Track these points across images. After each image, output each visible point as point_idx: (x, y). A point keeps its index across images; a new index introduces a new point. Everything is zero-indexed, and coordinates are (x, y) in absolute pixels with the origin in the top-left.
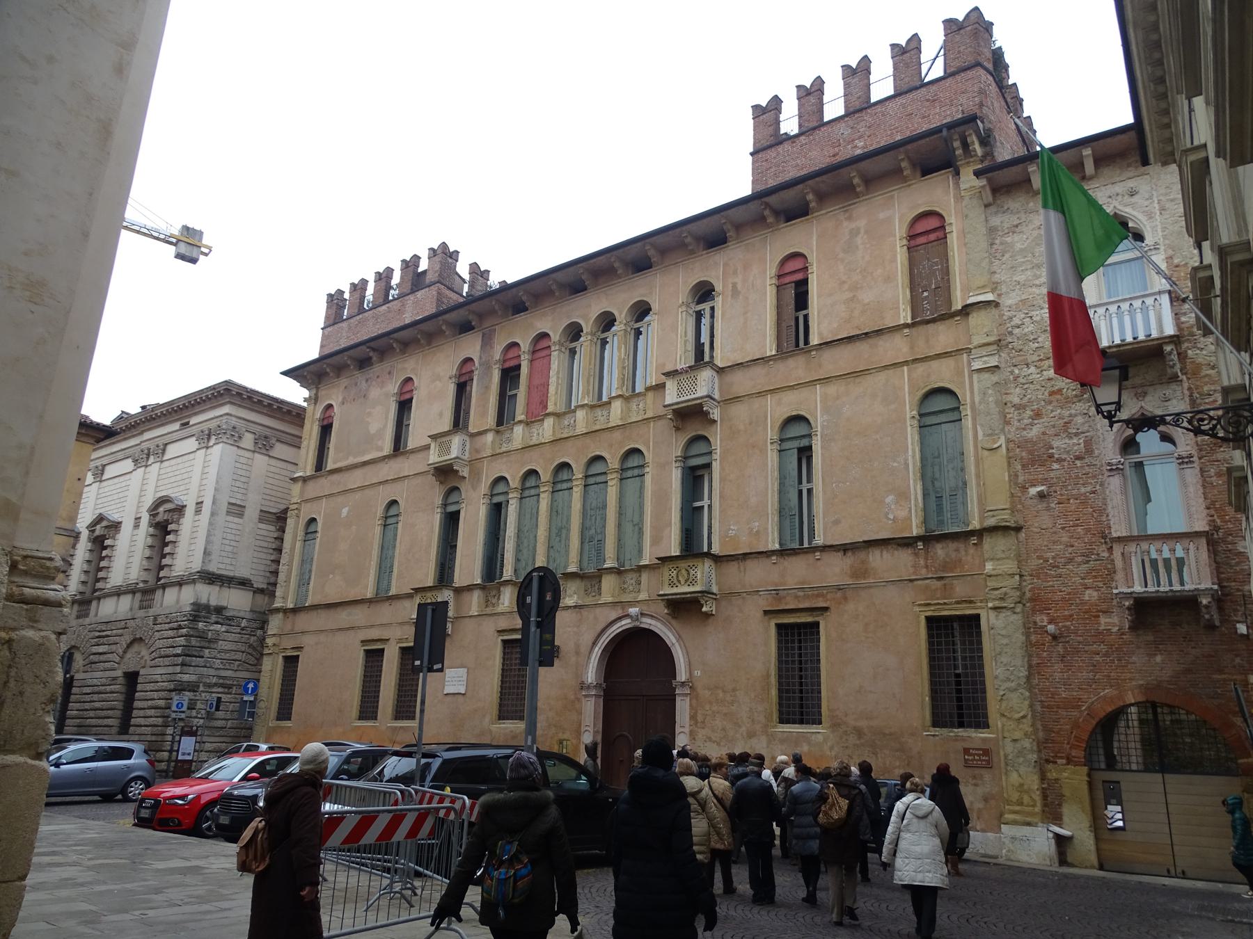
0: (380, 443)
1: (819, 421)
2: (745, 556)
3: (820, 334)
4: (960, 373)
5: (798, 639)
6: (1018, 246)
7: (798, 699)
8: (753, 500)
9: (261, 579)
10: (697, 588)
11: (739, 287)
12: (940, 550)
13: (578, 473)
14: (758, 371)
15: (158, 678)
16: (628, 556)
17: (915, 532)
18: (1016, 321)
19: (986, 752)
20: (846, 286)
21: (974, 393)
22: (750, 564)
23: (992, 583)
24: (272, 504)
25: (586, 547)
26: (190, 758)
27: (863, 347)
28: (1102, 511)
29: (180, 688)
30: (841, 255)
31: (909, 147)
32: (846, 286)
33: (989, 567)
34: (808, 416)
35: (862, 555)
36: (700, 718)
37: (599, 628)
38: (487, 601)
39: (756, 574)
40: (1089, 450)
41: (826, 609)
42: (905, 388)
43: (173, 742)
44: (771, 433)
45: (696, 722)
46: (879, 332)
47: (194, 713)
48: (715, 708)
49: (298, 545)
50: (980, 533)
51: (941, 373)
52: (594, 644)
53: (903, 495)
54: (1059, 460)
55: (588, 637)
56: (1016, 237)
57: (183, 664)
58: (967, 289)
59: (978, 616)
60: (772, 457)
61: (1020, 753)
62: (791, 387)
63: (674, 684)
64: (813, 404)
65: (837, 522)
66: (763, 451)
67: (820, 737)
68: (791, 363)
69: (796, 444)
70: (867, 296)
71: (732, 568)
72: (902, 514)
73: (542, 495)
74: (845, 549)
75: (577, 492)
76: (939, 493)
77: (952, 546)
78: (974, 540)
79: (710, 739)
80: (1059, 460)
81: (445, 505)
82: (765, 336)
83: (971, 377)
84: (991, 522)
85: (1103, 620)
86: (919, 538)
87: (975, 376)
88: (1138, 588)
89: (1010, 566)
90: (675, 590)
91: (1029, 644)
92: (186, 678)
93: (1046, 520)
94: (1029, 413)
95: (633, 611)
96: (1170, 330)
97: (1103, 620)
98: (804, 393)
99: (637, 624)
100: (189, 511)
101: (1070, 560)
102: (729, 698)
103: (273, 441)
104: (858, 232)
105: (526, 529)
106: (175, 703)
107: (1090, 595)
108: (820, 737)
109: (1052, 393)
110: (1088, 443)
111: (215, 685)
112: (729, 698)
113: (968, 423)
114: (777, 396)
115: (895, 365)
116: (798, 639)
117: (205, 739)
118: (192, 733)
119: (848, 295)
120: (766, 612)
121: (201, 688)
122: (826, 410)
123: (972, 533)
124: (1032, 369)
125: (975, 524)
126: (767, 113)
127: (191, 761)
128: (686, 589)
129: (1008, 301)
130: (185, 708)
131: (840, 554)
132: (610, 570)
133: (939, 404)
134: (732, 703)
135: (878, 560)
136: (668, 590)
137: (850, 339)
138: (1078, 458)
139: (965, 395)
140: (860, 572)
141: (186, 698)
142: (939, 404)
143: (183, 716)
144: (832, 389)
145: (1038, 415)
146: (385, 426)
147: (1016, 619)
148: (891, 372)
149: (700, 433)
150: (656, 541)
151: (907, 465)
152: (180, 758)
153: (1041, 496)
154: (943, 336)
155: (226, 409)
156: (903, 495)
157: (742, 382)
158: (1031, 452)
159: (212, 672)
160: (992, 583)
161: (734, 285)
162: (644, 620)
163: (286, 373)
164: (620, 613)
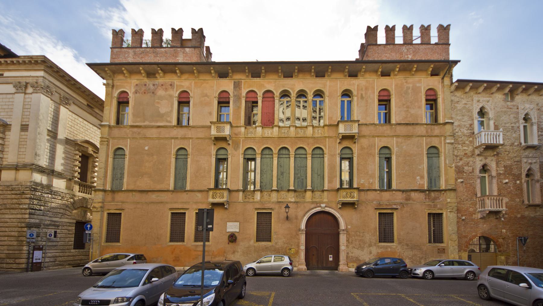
0: (169, 119)
1: (395, 150)
2: (368, 190)
3: (396, 120)
4: (441, 143)
5: (386, 218)
6: (458, 108)
7: (386, 234)
8: (370, 172)
9: (69, 174)
10: (355, 199)
11: (364, 95)
12: (433, 194)
13: (292, 152)
14: (372, 128)
15: (8, 220)
16: (316, 186)
17: (426, 188)
18: (457, 131)
19: (444, 249)
20: (405, 106)
21: (445, 150)
22: (369, 192)
23: (449, 205)
24: (72, 136)
25: (296, 181)
26: (40, 261)
27: (410, 127)
28: (475, 188)
29: (30, 226)
30: (403, 95)
31: (437, 64)
32: (405, 106)
33: (449, 200)
34: (391, 147)
35: (409, 193)
36: (350, 241)
37: (306, 210)
38: (246, 197)
39: (371, 195)
40: (473, 171)
41: (397, 209)
42: (425, 144)
43: (29, 253)
44: (377, 151)
45: (349, 242)
46: (417, 124)
47: (39, 239)
48: (356, 238)
49: (110, 160)
50: (445, 190)
51: (435, 142)
52: (304, 216)
53: (422, 177)
54: (466, 173)
55: (300, 213)
56: (458, 105)
57: (30, 214)
58: (445, 117)
59: (442, 214)
60: (377, 159)
61: (454, 249)
62: (385, 136)
63: (339, 230)
64: (393, 143)
65: (400, 183)
66: (374, 156)
67: (395, 247)
68: (385, 128)
69: (384, 156)
70: (412, 111)
71: (363, 193)
72: (422, 183)
73: (274, 158)
74: (403, 191)
75: (292, 160)
76: (433, 178)
77: (436, 193)
78: (443, 192)
79: (354, 247)
80: (466, 173)
81: (217, 155)
82: (374, 116)
83: (445, 146)
84: (450, 188)
85: (474, 216)
86: (426, 190)
87: (447, 145)
88: (490, 208)
89: (454, 200)
90: (345, 199)
91: (458, 222)
92: (32, 221)
93: (461, 189)
94: (458, 158)
95: (323, 205)
96: (501, 142)
97: (474, 216)
98: (390, 139)
99: (323, 210)
100: (15, 129)
101: (467, 200)
102: (361, 234)
103: (71, 102)
104: (409, 89)
105: (265, 171)
106: (29, 234)
107: (471, 209)
108: (395, 247)
109: (465, 154)
110: (473, 169)
111: (50, 225)
112: (361, 234)
113: (442, 158)
114: (380, 138)
115: (422, 136)
116: (386, 218)
117: (47, 251)
118: (40, 249)
119: (405, 109)
120: (376, 209)
121: (42, 226)
122: (397, 146)
123: (442, 190)
124: (460, 146)
125: (443, 187)
126: (371, 32)
127: (41, 263)
128: (350, 199)
129: (456, 124)
130: (35, 237)
131: (401, 193)
132: (258, 190)
133: (433, 152)
134: (363, 236)
135: (413, 194)
136: (342, 199)
137: (407, 124)
138: (470, 173)
139: (442, 150)
140: (408, 199)
141: (35, 232)
142: (433, 152)
143: (34, 240)
144: (400, 140)
145: (461, 159)
146: (172, 111)
147: (456, 215)
148: (420, 138)
149: (305, 147)
150: (330, 182)
151: (424, 168)
152: (34, 261)
153: (462, 182)
154: (437, 130)
155: (41, 73)
156: (422, 177)
157: (366, 131)
158: (459, 170)
159: (47, 218)
160: (449, 205)
161: (362, 95)
162: (326, 208)
163: (377, 26)
164: (315, 205)
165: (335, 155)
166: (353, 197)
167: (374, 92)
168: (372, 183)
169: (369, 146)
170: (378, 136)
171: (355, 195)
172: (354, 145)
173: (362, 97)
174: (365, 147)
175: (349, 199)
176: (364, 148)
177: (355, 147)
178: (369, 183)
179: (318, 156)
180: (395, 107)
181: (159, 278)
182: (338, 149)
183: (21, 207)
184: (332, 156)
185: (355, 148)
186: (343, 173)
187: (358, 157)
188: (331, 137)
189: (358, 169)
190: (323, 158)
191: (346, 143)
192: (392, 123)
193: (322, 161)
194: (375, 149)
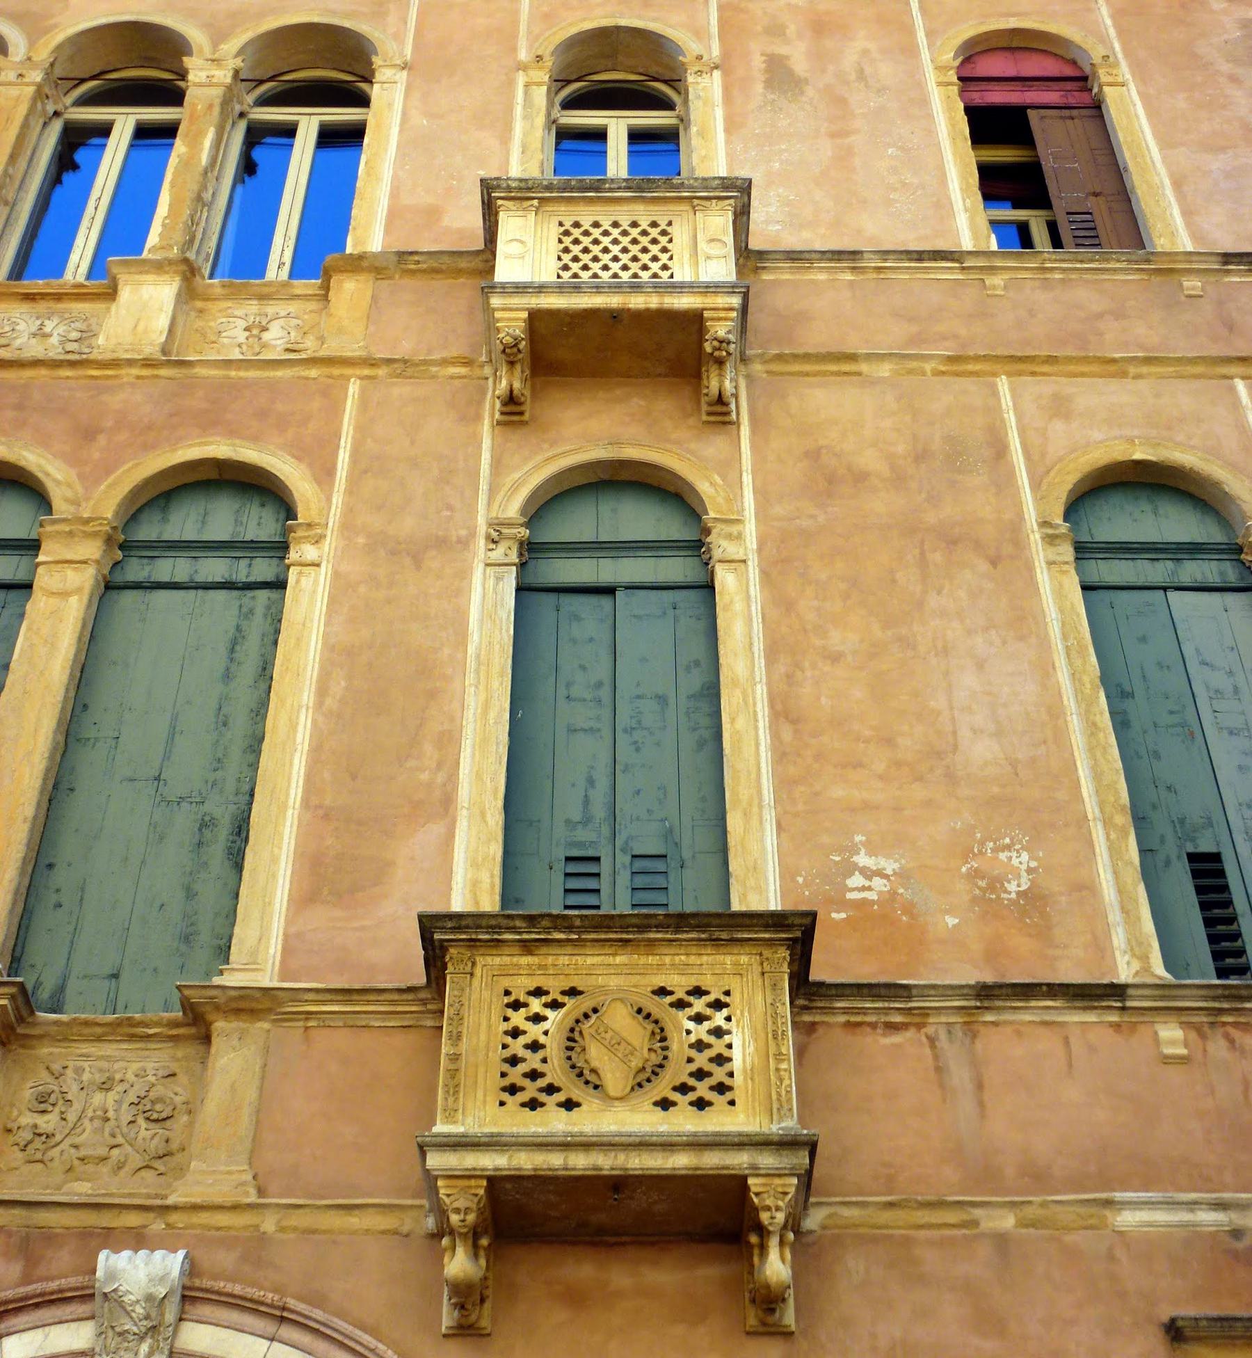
8: (981, 752)
66: (1004, 554)
165: (449, 545)
166: (707, 1082)
167: (911, 51)
168: (1033, 899)
169: (921, 456)
170: (1020, 363)
171: (742, 1048)
172: (715, 446)
173: (779, 75)
174: (870, 460)
175: (621, 1127)
176: (860, 477)
177: (730, 466)
178: (987, 896)
179: (215, 568)
180: (1166, 144)
181: (1175, 977)
182: (502, 479)
183: (771, 1041)
184: (407, 552)
185: (736, 482)
186: (200, 578)
187: (779, 564)
188: (403, 367)
189: (784, 712)
190: (279, 585)
191: (596, 427)
192: (1161, 243)
193: (256, 627)
194: (1004, 483)
